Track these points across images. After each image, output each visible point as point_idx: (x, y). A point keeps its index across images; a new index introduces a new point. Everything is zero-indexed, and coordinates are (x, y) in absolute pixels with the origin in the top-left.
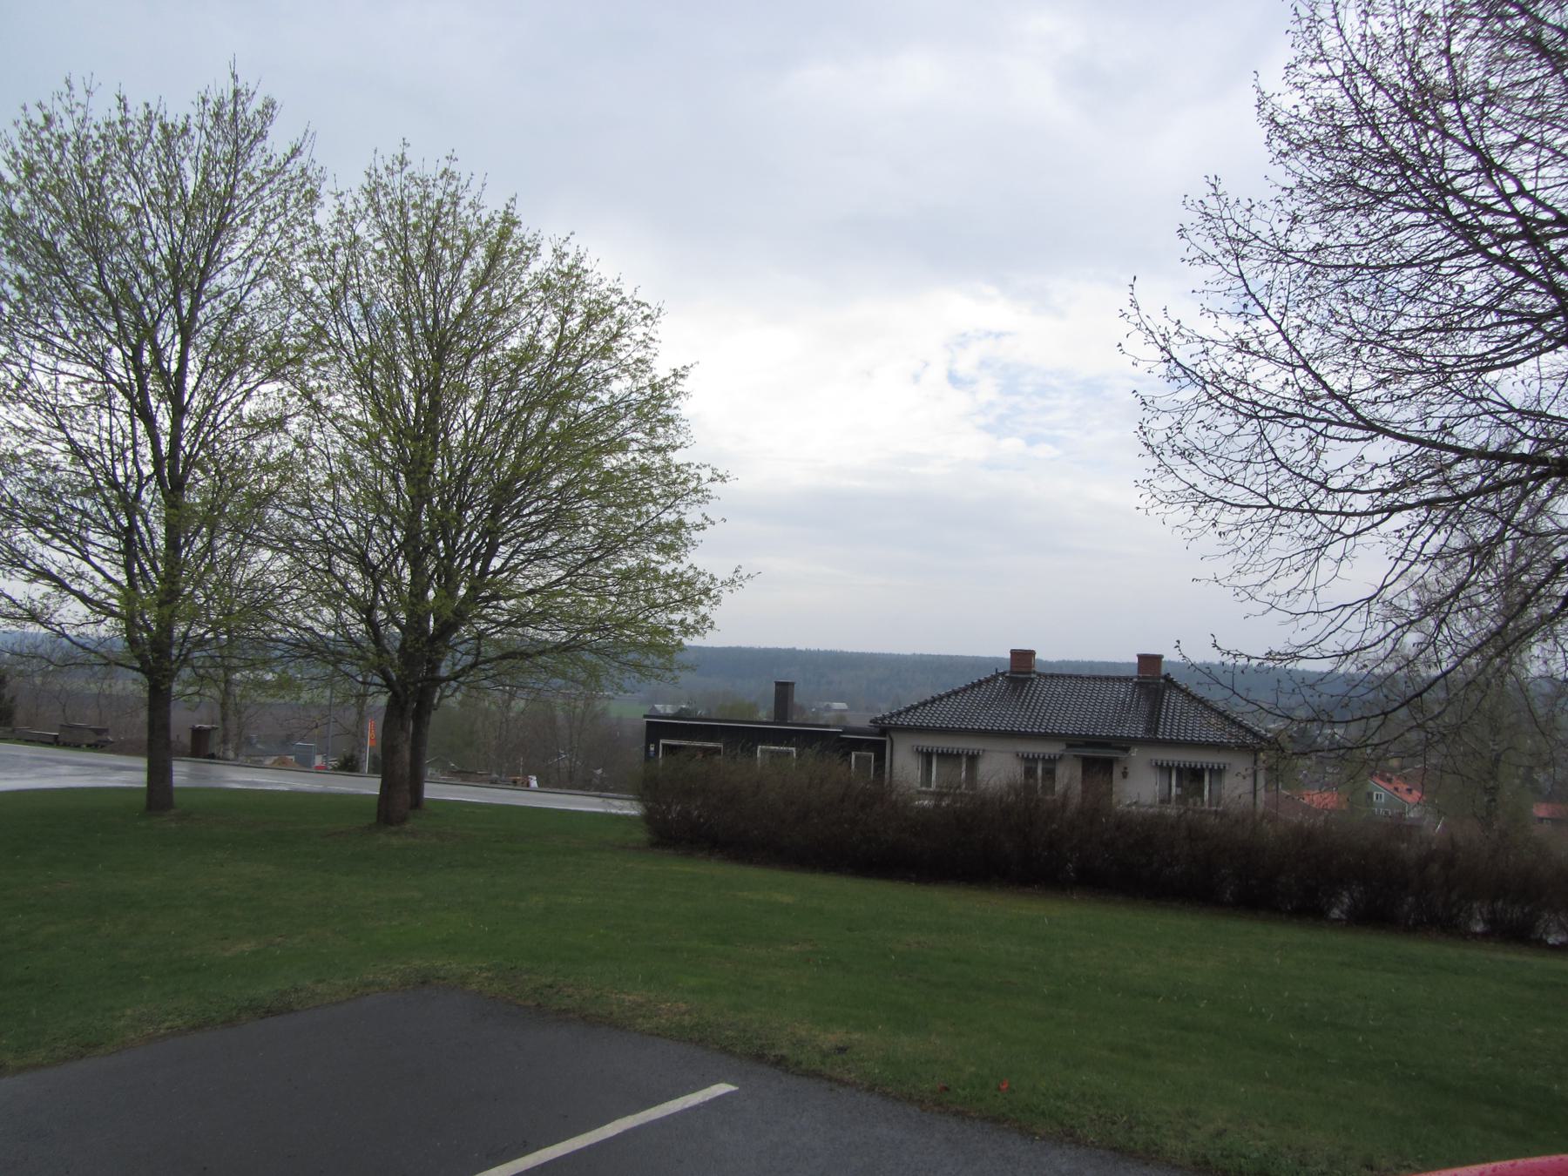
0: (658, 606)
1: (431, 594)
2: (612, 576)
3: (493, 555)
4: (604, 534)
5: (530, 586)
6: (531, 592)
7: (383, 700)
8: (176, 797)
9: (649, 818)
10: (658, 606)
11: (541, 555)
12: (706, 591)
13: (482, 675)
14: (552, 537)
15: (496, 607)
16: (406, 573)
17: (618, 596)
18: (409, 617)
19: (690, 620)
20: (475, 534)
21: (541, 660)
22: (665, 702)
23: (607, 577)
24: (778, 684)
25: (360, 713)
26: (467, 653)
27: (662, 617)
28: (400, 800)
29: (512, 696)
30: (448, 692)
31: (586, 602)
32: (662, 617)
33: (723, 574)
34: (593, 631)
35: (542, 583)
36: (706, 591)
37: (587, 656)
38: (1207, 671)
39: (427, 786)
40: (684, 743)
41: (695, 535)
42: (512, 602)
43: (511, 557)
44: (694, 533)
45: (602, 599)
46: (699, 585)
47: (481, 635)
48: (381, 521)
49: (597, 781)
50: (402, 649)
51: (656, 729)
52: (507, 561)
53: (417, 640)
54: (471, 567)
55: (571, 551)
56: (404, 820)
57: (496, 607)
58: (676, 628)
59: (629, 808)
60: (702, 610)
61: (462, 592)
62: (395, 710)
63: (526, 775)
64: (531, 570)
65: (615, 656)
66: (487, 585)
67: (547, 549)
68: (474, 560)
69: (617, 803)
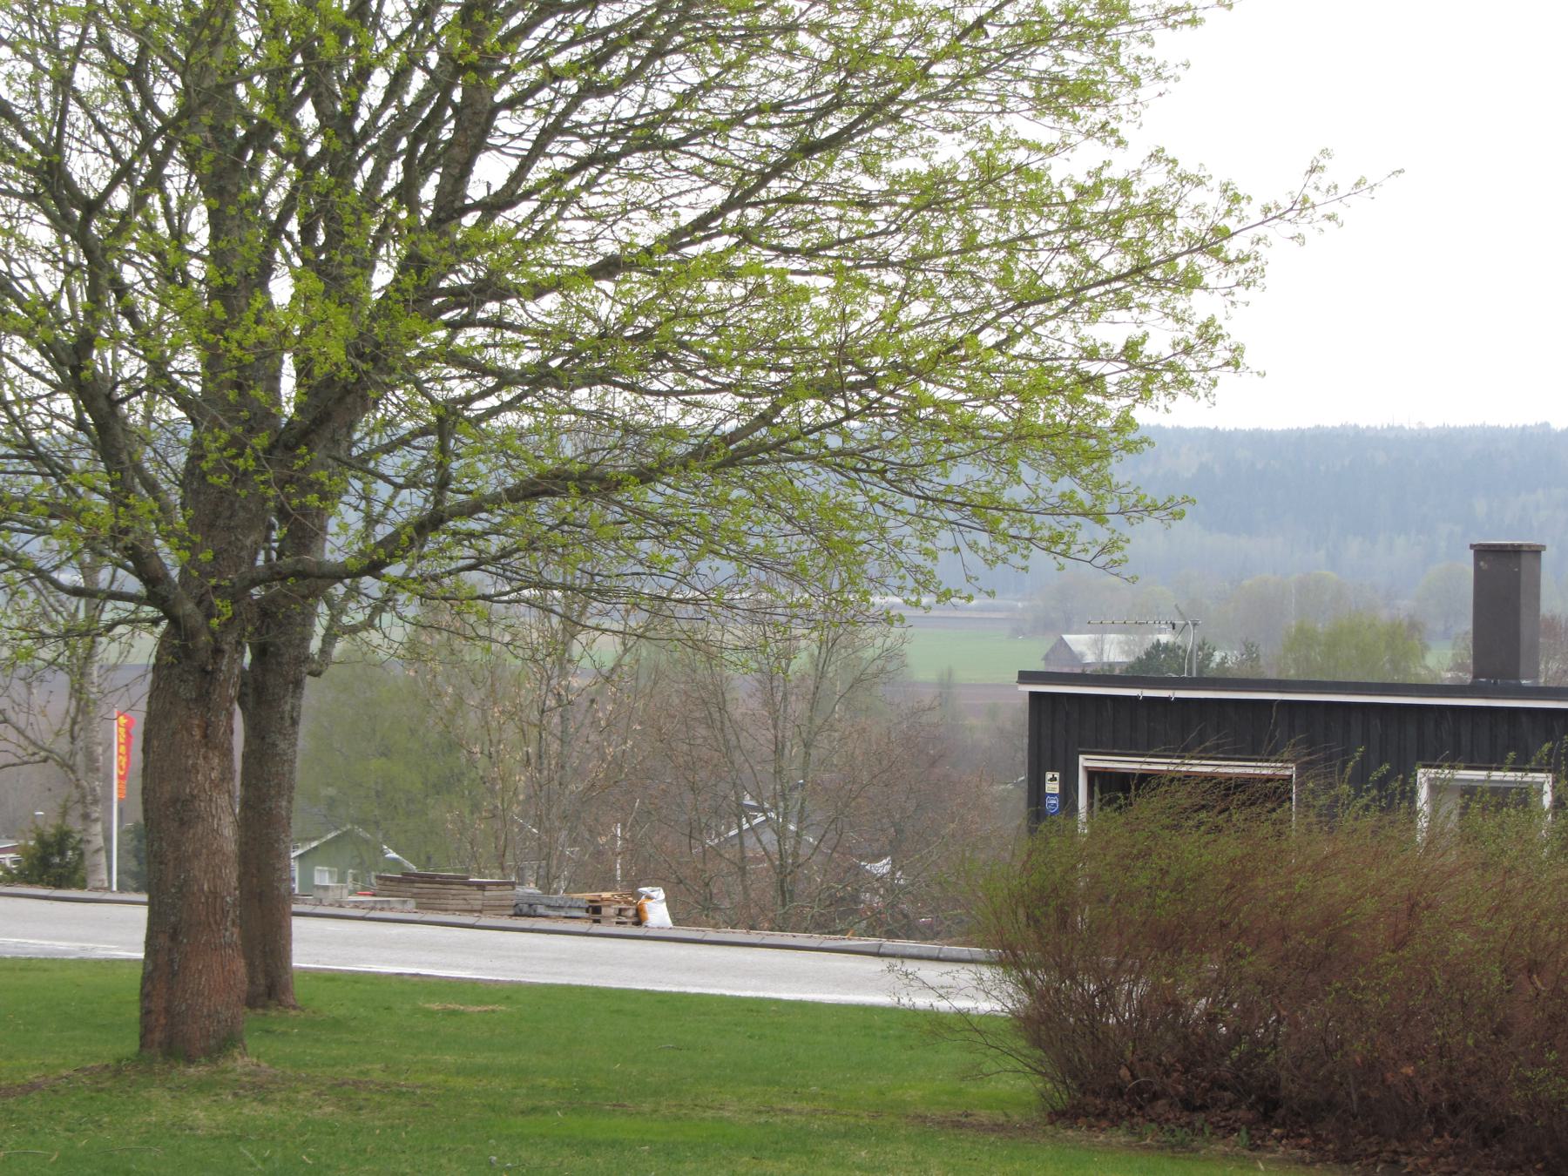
0: (1049, 296)
1: (281, 289)
2: (888, 197)
3: (479, 146)
4: (852, 59)
5: (608, 247)
6: (609, 267)
7: (145, 646)
8: (299, 991)
9: (1041, 1025)
10: (1049, 296)
11: (645, 137)
12: (1212, 243)
13: (464, 553)
14: (681, 73)
15: (497, 323)
16: (198, 224)
17: (910, 265)
18: (213, 362)
19: (1159, 345)
20: (418, 80)
21: (653, 497)
22: (1101, 627)
23: (866, 204)
24: (1482, 552)
25: (78, 691)
26: (412, 483)
27: (1061, 337)
28: (214, 965)
29: (572, 625)
30: (355, 615)
31: (804, 294)
32: (1061, 337)
33: (1269, 183)
34: (826, 391)
35: (646, 231)
36: (1212, 243)
37: (817, 482)
38: (1131, 666)
39: (300, 928)
40: (1159, 765)
41: (1169, 45)
42: (551, 301)
43: (539, 148)
44: (1161, 34)
45: (848, 281)
46: (1185, 222)
47: (448, 418)
48: (104, 44)
49: (872, 900)
50: (193, 477)
51: (1064, 718)
52: (526, 163)
53: (238, 444)
54: (407, 193)
55: (759, 110)
56: (227, 1042)
57: (497, 323)
58: (1113, 373)
59: (971, 990)
60: (1200, 305)
61: (383, 276)
62: (184, 673)
63: (633, 886)
64: (612, 190)
65: (903, 477)
66: (462, 251)
67: (666, 117)
68: (415, 174)
69: (930, 972)
